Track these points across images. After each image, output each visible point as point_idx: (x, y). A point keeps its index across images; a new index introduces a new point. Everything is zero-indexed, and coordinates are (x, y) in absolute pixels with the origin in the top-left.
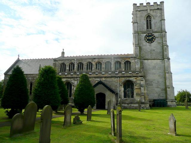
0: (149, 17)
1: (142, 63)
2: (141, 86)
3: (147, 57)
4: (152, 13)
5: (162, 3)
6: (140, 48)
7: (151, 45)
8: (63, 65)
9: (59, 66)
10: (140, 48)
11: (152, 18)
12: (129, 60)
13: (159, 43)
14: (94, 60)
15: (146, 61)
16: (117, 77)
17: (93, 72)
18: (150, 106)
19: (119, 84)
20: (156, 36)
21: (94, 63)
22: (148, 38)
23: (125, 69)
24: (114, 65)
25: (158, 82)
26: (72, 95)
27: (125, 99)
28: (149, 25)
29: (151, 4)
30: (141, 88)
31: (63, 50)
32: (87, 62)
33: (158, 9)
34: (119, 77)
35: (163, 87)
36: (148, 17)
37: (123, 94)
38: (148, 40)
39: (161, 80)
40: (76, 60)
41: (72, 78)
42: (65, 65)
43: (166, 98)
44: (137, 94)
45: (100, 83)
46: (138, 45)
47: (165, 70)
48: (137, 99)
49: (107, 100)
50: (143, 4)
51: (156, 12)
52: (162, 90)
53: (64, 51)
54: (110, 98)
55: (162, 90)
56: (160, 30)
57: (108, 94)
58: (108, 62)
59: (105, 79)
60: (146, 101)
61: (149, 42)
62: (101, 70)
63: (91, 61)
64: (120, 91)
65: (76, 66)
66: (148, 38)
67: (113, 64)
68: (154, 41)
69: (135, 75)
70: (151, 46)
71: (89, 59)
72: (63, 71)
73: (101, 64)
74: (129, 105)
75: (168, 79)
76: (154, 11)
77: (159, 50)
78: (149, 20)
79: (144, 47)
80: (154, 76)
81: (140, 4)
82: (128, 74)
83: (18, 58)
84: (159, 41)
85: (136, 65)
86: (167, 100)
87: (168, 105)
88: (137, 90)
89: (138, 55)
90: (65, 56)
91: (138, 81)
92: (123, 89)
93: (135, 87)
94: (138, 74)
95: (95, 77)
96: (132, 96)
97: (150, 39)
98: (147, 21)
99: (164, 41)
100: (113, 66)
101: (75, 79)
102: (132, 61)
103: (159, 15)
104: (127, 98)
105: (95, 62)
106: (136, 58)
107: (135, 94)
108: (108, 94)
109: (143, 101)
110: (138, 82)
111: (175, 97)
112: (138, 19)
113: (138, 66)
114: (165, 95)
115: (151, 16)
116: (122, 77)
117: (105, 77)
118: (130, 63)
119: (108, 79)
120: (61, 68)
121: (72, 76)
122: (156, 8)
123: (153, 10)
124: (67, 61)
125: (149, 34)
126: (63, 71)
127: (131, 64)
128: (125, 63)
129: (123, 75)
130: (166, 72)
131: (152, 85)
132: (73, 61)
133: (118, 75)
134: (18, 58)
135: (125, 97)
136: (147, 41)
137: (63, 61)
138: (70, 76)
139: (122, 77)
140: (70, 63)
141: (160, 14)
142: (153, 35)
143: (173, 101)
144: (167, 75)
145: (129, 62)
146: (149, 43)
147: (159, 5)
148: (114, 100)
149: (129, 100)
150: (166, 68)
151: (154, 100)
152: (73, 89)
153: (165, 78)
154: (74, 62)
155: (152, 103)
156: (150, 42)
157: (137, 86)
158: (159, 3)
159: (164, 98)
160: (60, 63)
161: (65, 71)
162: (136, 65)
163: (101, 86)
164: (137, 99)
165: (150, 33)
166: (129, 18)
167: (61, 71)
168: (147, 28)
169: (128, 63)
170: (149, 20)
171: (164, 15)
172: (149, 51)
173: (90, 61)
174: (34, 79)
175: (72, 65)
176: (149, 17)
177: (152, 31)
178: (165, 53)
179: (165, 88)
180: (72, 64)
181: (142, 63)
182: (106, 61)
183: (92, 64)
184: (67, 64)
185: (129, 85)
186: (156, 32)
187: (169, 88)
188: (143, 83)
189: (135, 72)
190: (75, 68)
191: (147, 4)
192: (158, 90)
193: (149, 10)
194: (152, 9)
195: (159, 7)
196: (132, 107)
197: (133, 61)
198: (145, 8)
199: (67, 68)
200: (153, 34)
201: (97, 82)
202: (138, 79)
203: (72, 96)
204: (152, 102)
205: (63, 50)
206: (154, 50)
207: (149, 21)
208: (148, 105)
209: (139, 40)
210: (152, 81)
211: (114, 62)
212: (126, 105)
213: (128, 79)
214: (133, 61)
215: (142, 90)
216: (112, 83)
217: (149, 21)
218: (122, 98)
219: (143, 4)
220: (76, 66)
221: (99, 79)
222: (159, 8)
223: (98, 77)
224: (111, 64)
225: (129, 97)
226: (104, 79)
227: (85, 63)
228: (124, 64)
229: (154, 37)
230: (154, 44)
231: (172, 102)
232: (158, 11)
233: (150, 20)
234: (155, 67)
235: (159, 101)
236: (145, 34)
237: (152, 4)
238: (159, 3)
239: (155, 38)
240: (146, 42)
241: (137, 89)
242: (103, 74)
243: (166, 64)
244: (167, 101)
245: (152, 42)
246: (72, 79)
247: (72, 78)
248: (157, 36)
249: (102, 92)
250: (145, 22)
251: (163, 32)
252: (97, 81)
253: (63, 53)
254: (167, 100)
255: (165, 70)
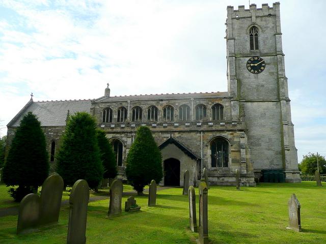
0: (255, 29)
1: (242, 108)
2: (241, 146)
3: (251, 98)
4: (259, 22)
5: (277, 5)
6: (240, 83)
7: (257, 76)
8: (108, 111)
9: (101, 113)
10: (240, 83)
11: (260, 30)
12: (220, 102)
13: (272, 74)
14: (161, 102)
15: (249, 104)
16: (200, 132)
17: (158, 123)
18: (256, 181)
19: (203, 143)
20: (266, 62)
21: (160, 108)
22: (252, 65)
23: (214, 118)
24: (195, 110)
25: (270, 140)
26: (123, 162)
27: (213, 168)
28: (254, 42)
29: (258, 7)
30: (241, 150)
31: (108, 85)
32: (148, 106)
33: (270, 15)
34: (203, 131)
35: (279, 149)
36: (252, 29)
37: (209, 161)
38: (253, 68)
39: (275, 137)
40: (129, 102)
41: (123, 132)
42: (111, 111)
43: (284, 168)
44: (233, 161)
45: (171, 141)
46: (235, 78)
47: (281, 120)
48: (234, 168)
49: (183, 170)
50: (243, 6)
51: (266, 21)
52: (277, 154)
53: (109, 88)
54: (188, 167)
55: (277, 154)
56: (272, 51)
57: (184, 160)
58: (185, 106)
59: (180, 135)
60: (250, 172)
61: (254, 71)
62: (172, 119)
63: (155, 105)
64: (205, 155)
65: (129, 112)
66: (252, 65)
67: (193, 109)
68: (262, 70)
69: (230, 128)
70: (258, 78)
71: (152, 100)
72: (107, 121)
73: (172, 109)
74: (221, 179)
75: (287, 136)
76: (263, 18)
77: (271, 85)
78: (254, 34)
79: (245, 81)
80: (263, 130)
81: (239, 7)
82: (219, 126)
83: (31, 99)
84: (272, 71)
85: (232, 110)
86: (286, 171)
87: (286, 179)
88: (234, 153)
89: (236, 94)
90: (112, 95)
91: (236, 139)
92: (209, 152)
93: (231, 149)
94: (235, 126)
95: (162, 132)
96: (226, 165)
97: (256, 66)
98: (251, 35)
99: (279, 69)
100: (194, 113)
101: (128, 134)
102: (226, 104)
103: (271, 25)
104: (217, 168)
105: (161, 105)
106: (232, 99)
107: (230, 160)
108: (184, 160)
109: (245, 172)
110: (236, 140)
111: (299, 165)
112: (236, 32)
113: (235, 113)
114: (281, 163)
115: (258, 27)
116: (208, 131)
117: (179, 132)
118: (222, 107)
119: (185, 135)
120: (104, 116)
121: (123, 130)
122: (267, 13)
123: (261, 17)
124: (114, 104)
125: (254, 59)
126: (107, 121)
127: (224, 109)
128: (213, 108)
129: (210, 129)
130: (284, 122)
131: (260, 145)
132: (124, 105)
133: (202, 129)
134: (31, 99)
135: (213, 165)
136: (251, 70)
137: (108, 104)
138: (119, 130)
139: (208, 131)
140: (120, 108)
141: (273, 23)
142: (261, 60)
143: (295, 172)
144: (285, 128)
145: (221, 105)
146: (254, 73)
147: (271, 8)
148: (194, 170)
149: (220, 170)
150: (283, 117)
151: (263, 171)
152: (125, 151)
153: (282, 134)
154: (126, 105)
155: (259, 176)
156: (256, 71)
157: (234, 146)
158: (271, 6)
159: (280, 167)
160: (102, 108)
161: (111, 121)
162: (232, 111)
163: (172, 146)
164: (234, 168)
165: (255, 57)
166: (221, 30)
167: (104, 121)
168: (252, 48)
169: (218, 107)
170: (254, 34)
171: (279, 26)
172: (255, 86)
173: (154, 103)
174: (59, 135)
175: (122, 110)
176: (255, 29)
177: (260, 52)
178: (282, 90)
179: (281, 149)
180: (123, 110)
181: (242, 108)
182: (181, 104)
183: (157, 109)
184: (115, 109)
185: (219, 145)
186: (266, 55)
187: (288, 150)
188: (243, 141)
189: (230, 123)
190: (128, 115)
191: (250, 6)
192: (270, 153)
193: (254, 18)
194: (260, 15)
195: (272, 12)
196: (225, 182)
197: (227, 104)
198: (248, 14)
199: (115, 116)
200: (262, 57)
201: (165, 139)
202: (235, 134)
203: (123, 164)
204: (259, 174)
205: (108, 85)
206: (263, 86)
207: (254, 37)
208: (253, 179)
209: (238, 68)
210: (260, 139)
211: (195, 106)
212: (215, 180)
213: (218, 134)
214: (227, 104)
215: (242, 153)
216: (191, 141)
217: (254, 37)
218: (209, 168)
219: (243, 6)
220: (129, 112)
221: (169, 136)
222: (272, 13)
223: (167, 132)
224: (189, 108)
225: (220, 165)
226: (177, 135)
227: (145, 108)
228: (212, 110)
229: (263, 63)
230: (263, 75)
231: (293, 173)
232: (270, 19)
233: (256, 35)
234: (265, 114)
235: (271, 173)
236: (248, 59)
237: (259, 6)
238: (271, 6)
239: (265, 65)
240: (250, 71)
241: (234, 151)
242: (176, 127)
243: (284, 110)
244: (285, 173)
245: (259, 72)
246: (123, 135)
247: (123, 132)
248: (268, 62)
249: (175, 157)
250: (248, 38)
251: (277, 55)
252: (165, 138)
253: (108, 91)
254: (286, 171)
255: (281, 120)
